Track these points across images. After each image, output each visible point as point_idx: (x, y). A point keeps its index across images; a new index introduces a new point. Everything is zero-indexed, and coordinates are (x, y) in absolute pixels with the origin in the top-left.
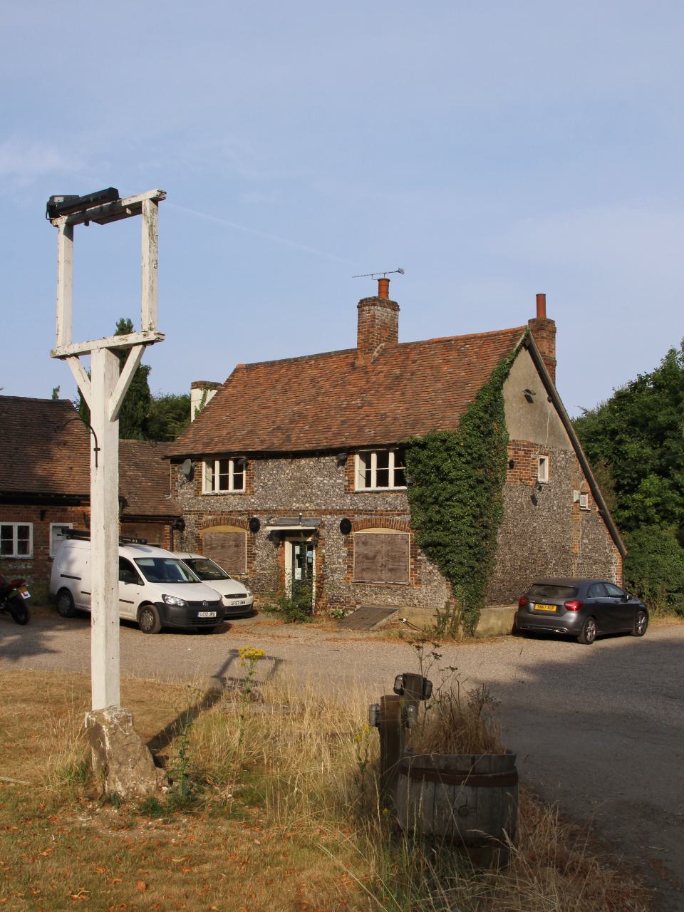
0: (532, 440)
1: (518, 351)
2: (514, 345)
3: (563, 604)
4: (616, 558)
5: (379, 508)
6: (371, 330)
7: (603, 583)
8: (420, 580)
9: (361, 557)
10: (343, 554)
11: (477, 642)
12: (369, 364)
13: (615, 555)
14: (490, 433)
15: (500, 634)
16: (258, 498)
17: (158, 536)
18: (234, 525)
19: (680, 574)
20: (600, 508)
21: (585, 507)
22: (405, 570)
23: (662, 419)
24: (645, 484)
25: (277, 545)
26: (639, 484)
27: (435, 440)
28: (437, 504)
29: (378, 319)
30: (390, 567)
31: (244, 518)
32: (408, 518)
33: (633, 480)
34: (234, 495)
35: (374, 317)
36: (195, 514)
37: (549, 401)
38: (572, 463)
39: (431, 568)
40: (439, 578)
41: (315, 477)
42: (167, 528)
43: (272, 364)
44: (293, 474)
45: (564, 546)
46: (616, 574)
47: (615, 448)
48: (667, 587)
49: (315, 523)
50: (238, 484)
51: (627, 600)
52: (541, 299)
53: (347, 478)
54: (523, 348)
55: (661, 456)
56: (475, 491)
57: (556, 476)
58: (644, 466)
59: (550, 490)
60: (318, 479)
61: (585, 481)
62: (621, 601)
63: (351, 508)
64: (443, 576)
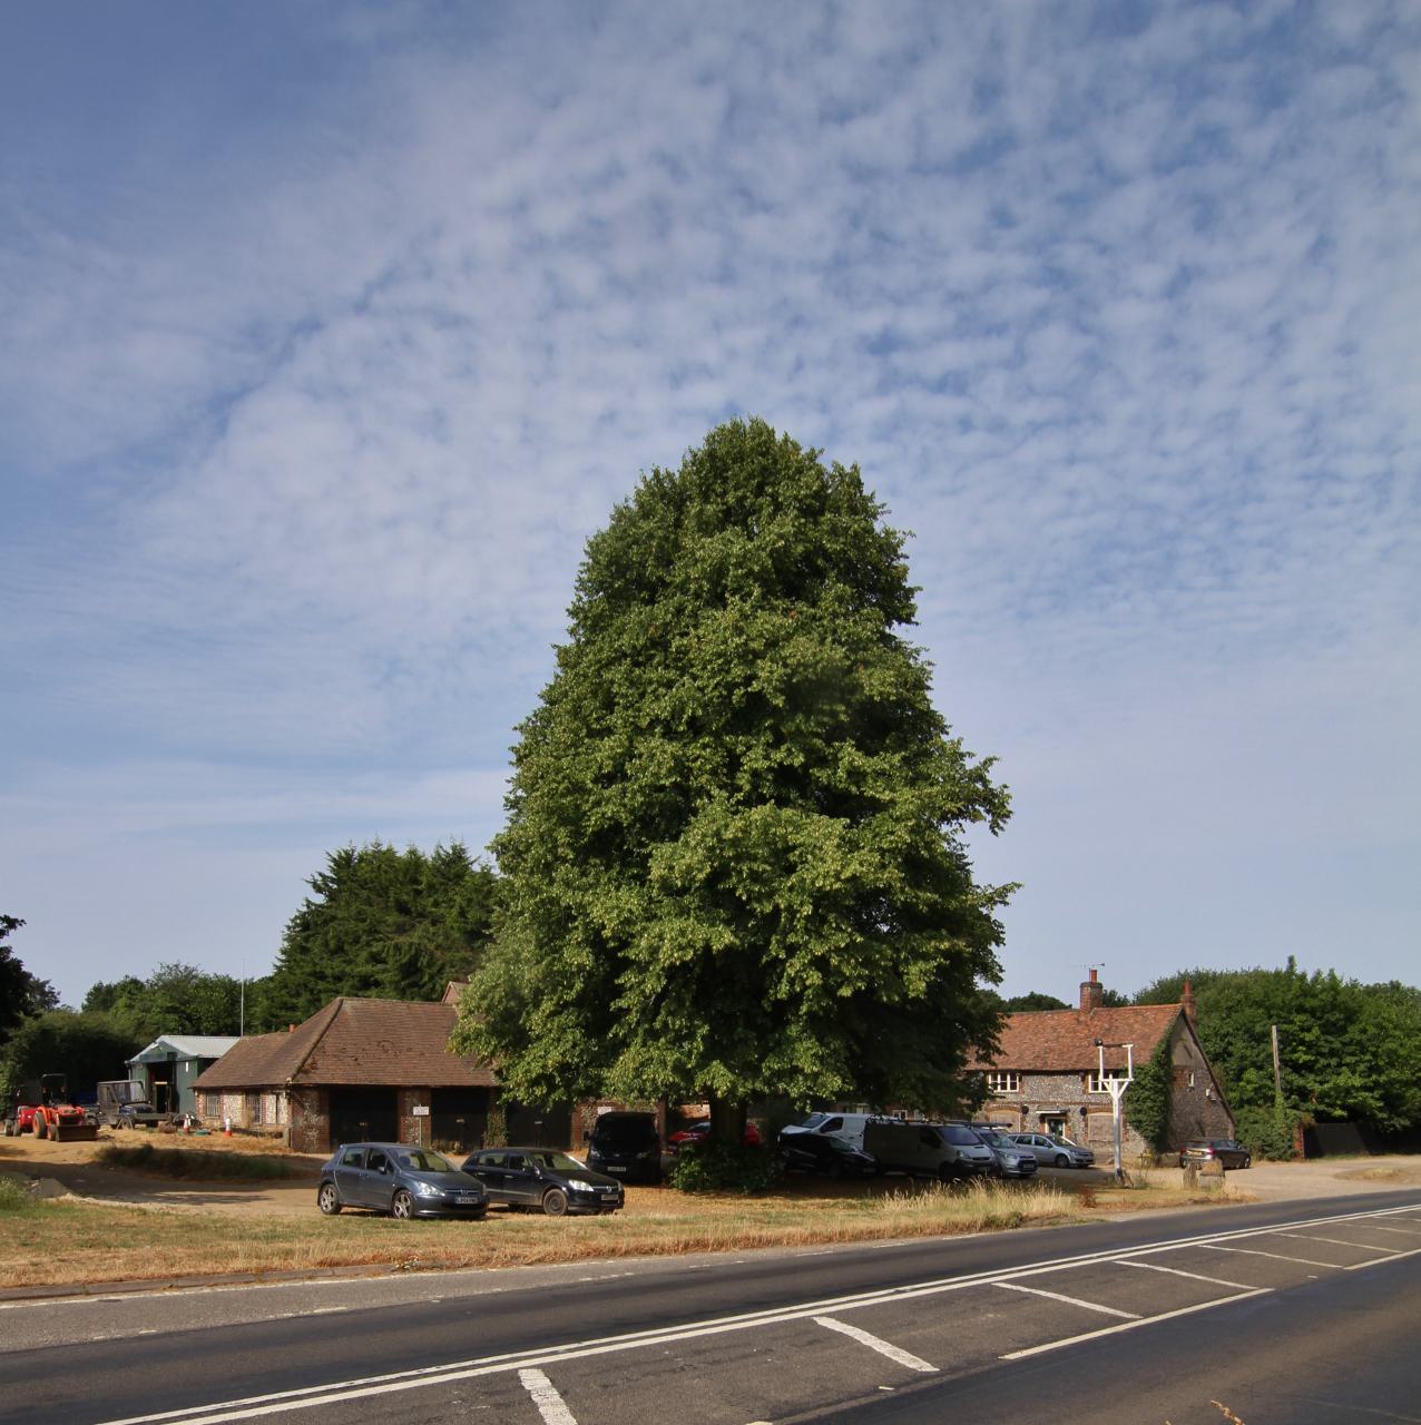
31: (1019, 1106)
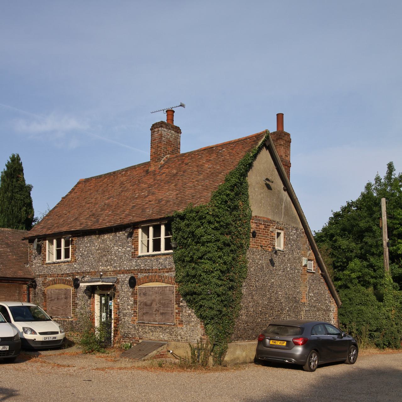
0: (270, 217)
1: (260, 149)
2: (257, 143)
3: (292, 340)
4: (334, 307)
5: (154, 268)
6: (159, 145)
7: (324, 324)
8: (182, 321)
9: (142, 304)
10: (131, 303)
11: (222, 370)
12: (157, 169)
13: (333, 305)
14: (236, 208)
15: (244, 363)
16: (78, 264)
17: (18, 292)
18: (64, 283)
19: (378, 319)
20: (322, 271)
21: (311, 270)
22: (172, 313)
23: (362, 224)
24: (352, 265)
25: (90, 297)
26: (347, 265)
27: (191, 211)
28: (193, 262)
29: (165, 137)
30: (161, 311)
31: (70, 278)
32: (173, 274)
33: (344, 263)
34: (64, 262)
35: (161, 135)
36: (42, 277)
37: (285, 190)
38: (302, 237)
39: (190, 312)
40: (195, 320)
41: (113, 247)
42: (25, 287)
43: (100, 177)
44: (99, 246)
45: (295, 298)
46: (334, 318)
47: (333, 245)
48: (369, 327)
49: (112, 280)
50: (67, 256)
51: (342, 337)
52: (280, 117)
53: (133, 246)
54: (264, 148)
55: (361, 248)
56: (223, 252)
57: (289, 246)
58: (351, 254)
59: (285, 256)
60: (115, 248)
61: (311, 251)
62: (338, 337)
63: (136, 268)
64: (198, 318)
